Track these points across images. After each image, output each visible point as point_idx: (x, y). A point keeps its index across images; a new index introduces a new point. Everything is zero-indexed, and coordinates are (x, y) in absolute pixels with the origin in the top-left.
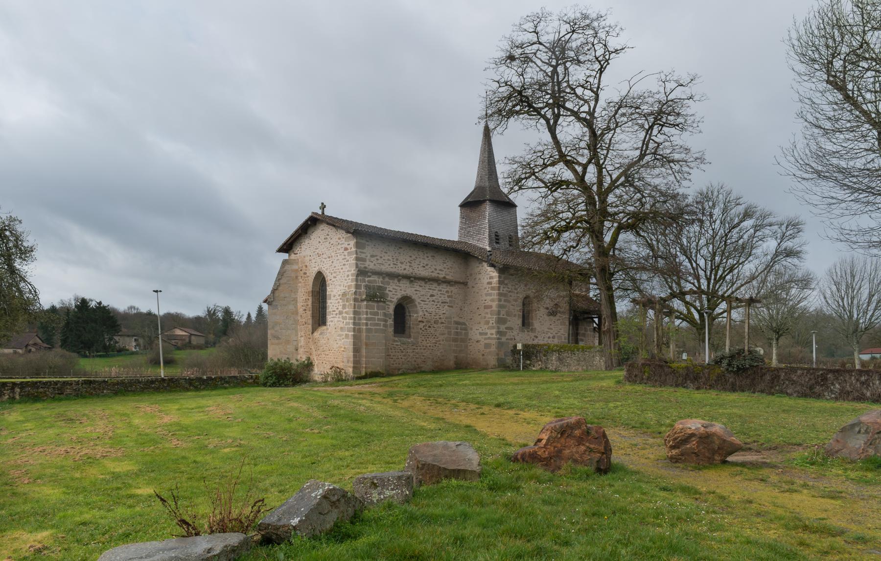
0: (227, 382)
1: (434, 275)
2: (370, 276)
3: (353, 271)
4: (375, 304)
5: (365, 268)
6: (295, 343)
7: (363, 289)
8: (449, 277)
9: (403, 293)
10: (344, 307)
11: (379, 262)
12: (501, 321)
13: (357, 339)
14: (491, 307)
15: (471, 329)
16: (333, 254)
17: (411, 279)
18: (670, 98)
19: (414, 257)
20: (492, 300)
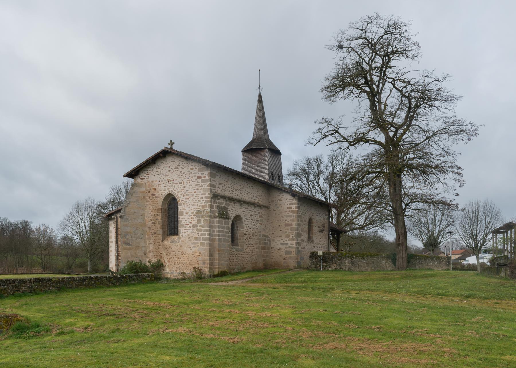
0: (134, 280)
1: (252, 200)
2: (219, 199)
3: (208, 194)
4: (223, 220)
5: (216, 192)
7: (215, 209)
8: (260, 203)
9: (237, 213)
10: (199, 221)
11: (224, 188)
12: (298, 235)
13: (211, 245)
14: (291, 225)
15: (273, 240)
16: (185, 181)
17: (241, 202)
18: (426, 88)
19: (242, 186)
20: (292, 220)
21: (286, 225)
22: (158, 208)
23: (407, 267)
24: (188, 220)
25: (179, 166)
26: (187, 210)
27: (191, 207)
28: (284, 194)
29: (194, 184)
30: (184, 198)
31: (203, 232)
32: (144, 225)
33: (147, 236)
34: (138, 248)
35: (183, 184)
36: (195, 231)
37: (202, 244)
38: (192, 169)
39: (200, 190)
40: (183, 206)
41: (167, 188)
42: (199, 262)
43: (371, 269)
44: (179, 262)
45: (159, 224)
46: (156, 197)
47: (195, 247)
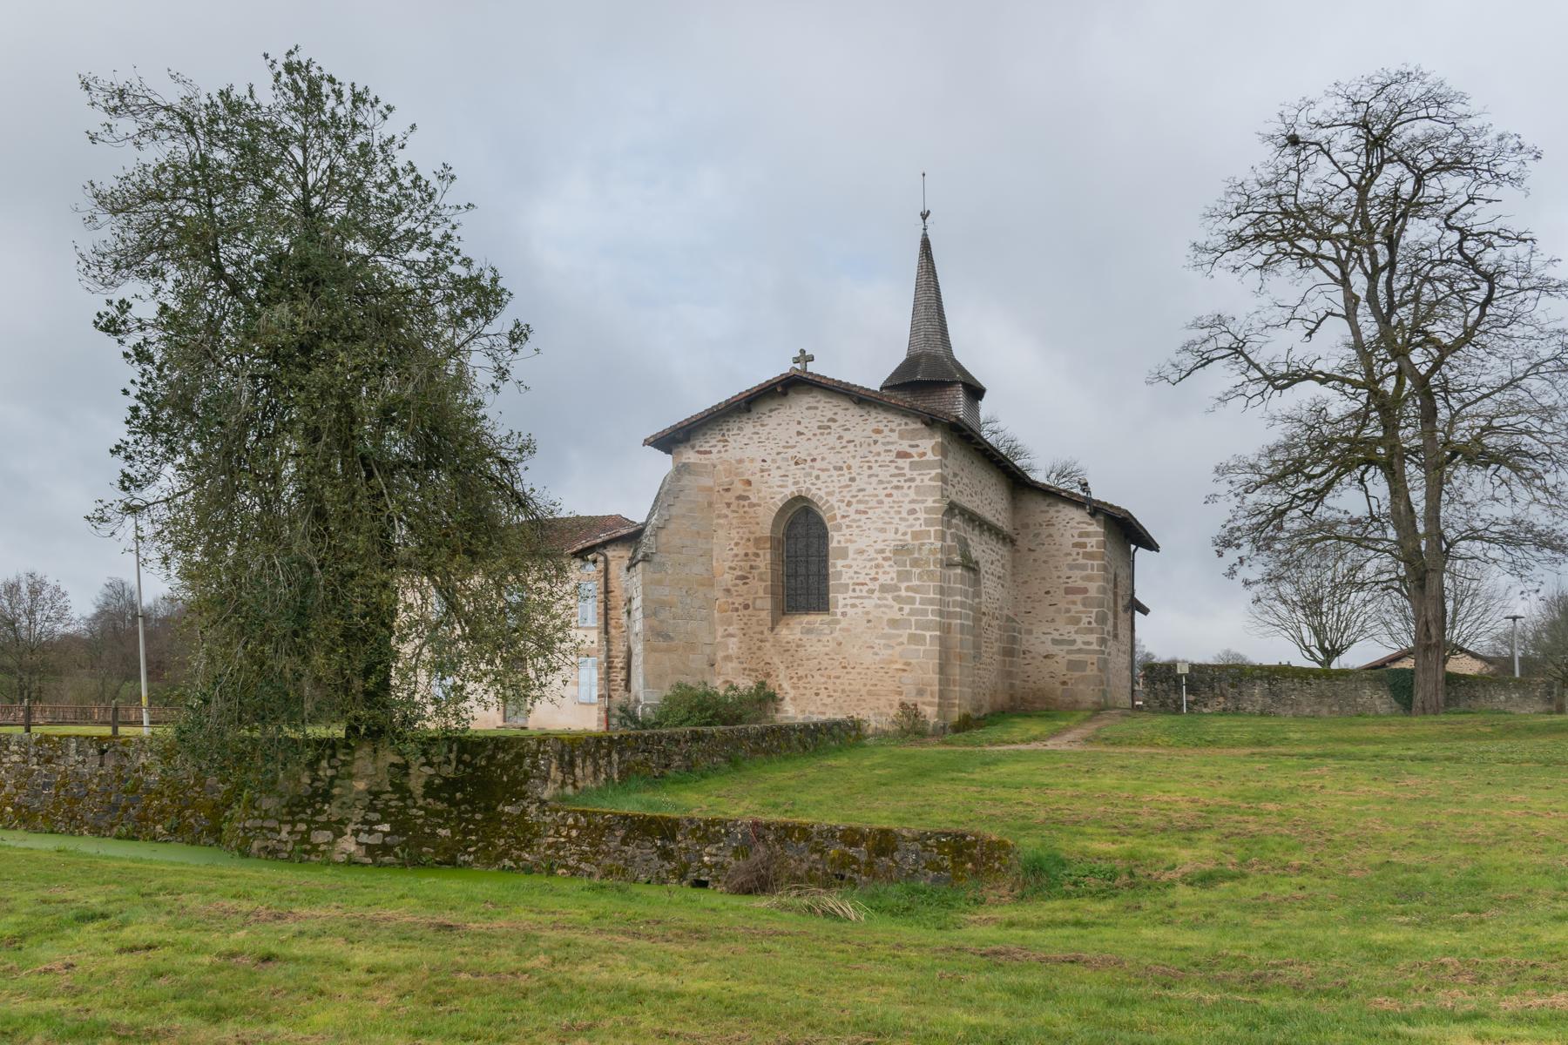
6: (708, 650)
7: (949, 542)
10: (903, 576)
13: (943, 642)
15: (1030, 632)
20: (1089, 578)
21: (1069, 591)
22: (758, 535)
23: (1447, 705)
24: (864, 572)
25: (834, 421)
26: (861, 543)
27: (875, 535)
28: (1061, 506)
29: (884, 474)
30: (851, 510)
31: (917, 606)
32: (709, 582)
33: (716, 615)
34: (691, 646)
35: (845, 471)
36: (890, 602)
37: (914, 639)
38: (878, 431)
39: (905, 490)
40: (845, 531)
41: (791, 480)
42: (904, 688)
43: (1331, 712)
44: (831, 687)
45: (761, 580)
46: (752, 505)
47: (887, 646)
